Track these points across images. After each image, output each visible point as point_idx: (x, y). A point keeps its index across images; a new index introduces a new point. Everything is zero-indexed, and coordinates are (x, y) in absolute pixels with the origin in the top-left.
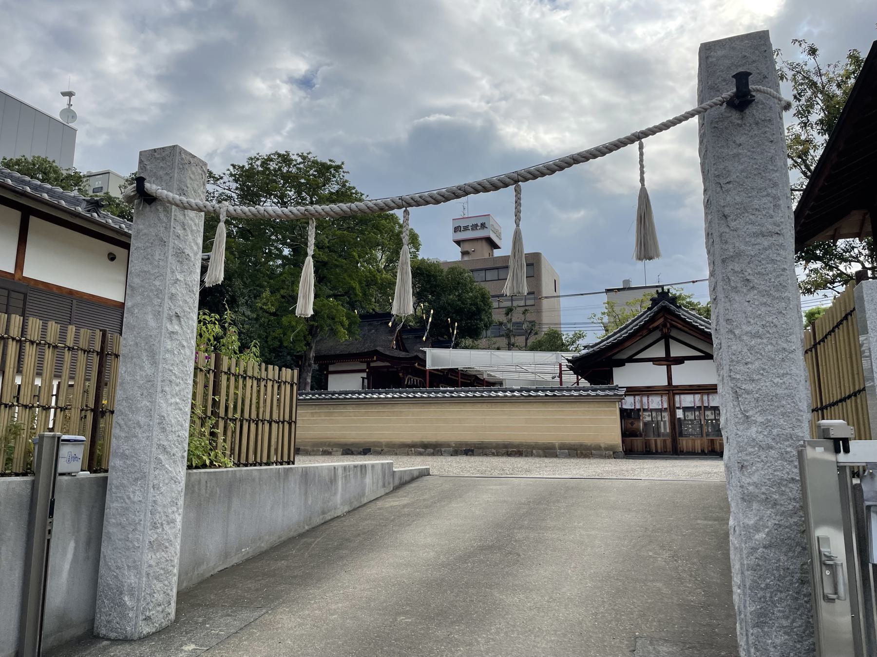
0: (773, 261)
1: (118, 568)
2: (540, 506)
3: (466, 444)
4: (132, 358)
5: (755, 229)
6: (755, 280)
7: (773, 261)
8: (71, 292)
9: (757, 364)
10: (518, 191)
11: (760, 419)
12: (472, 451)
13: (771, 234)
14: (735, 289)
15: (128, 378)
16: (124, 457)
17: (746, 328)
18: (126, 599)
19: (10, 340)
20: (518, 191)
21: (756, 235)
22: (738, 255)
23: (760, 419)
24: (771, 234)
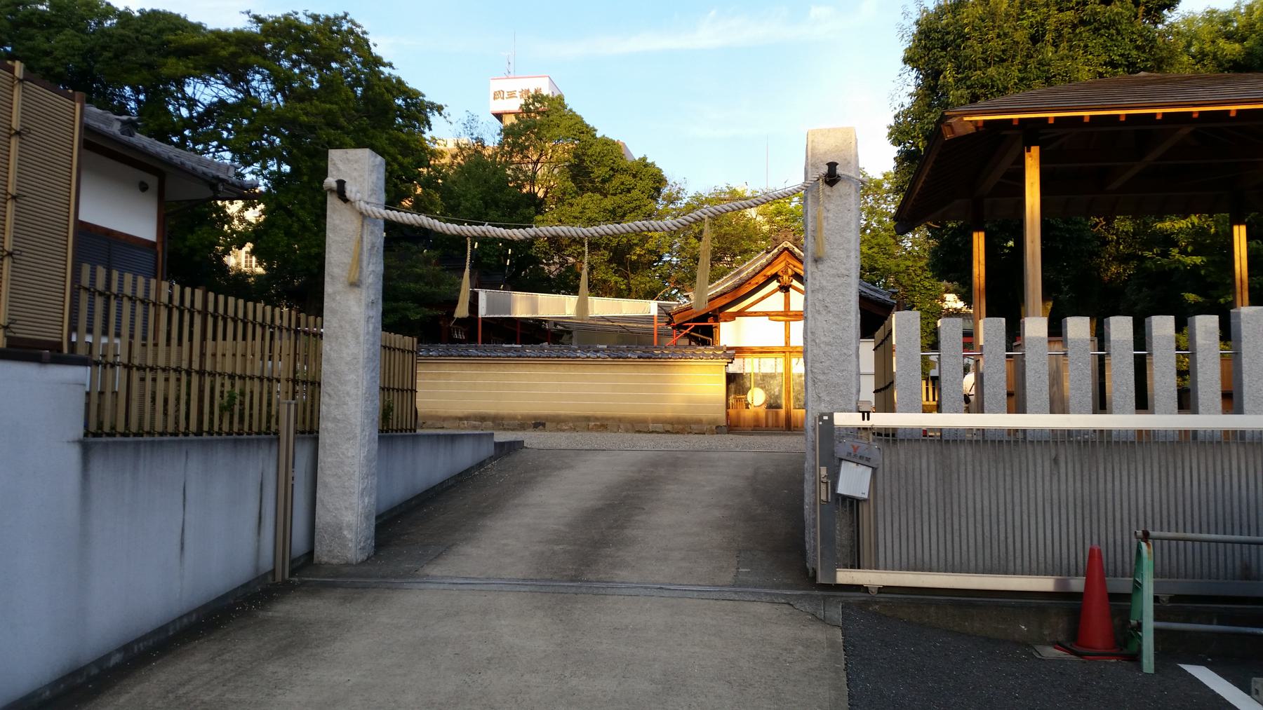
0: (843, 295)
1: (336, 509)
2: (674, 463)
3: (535, 418)
4: (337, 338)
5: (834, 272)
6: (832, 307)
7: (843, 295)
8: (108, 233)
9: (828, 363)
10: (787, 343)
11: (827, 399)
12: (544, 425)
13: (843, 276)
14: (819, 312)
15: (333, 355)
16: (335, 420)
17: (823, 339)
18: (345, 533)
19: (125, 299)
20: (787, 343)
21: (834, 276)
22: (822, 288)
23: (827, 399)
24: (843, 276)
